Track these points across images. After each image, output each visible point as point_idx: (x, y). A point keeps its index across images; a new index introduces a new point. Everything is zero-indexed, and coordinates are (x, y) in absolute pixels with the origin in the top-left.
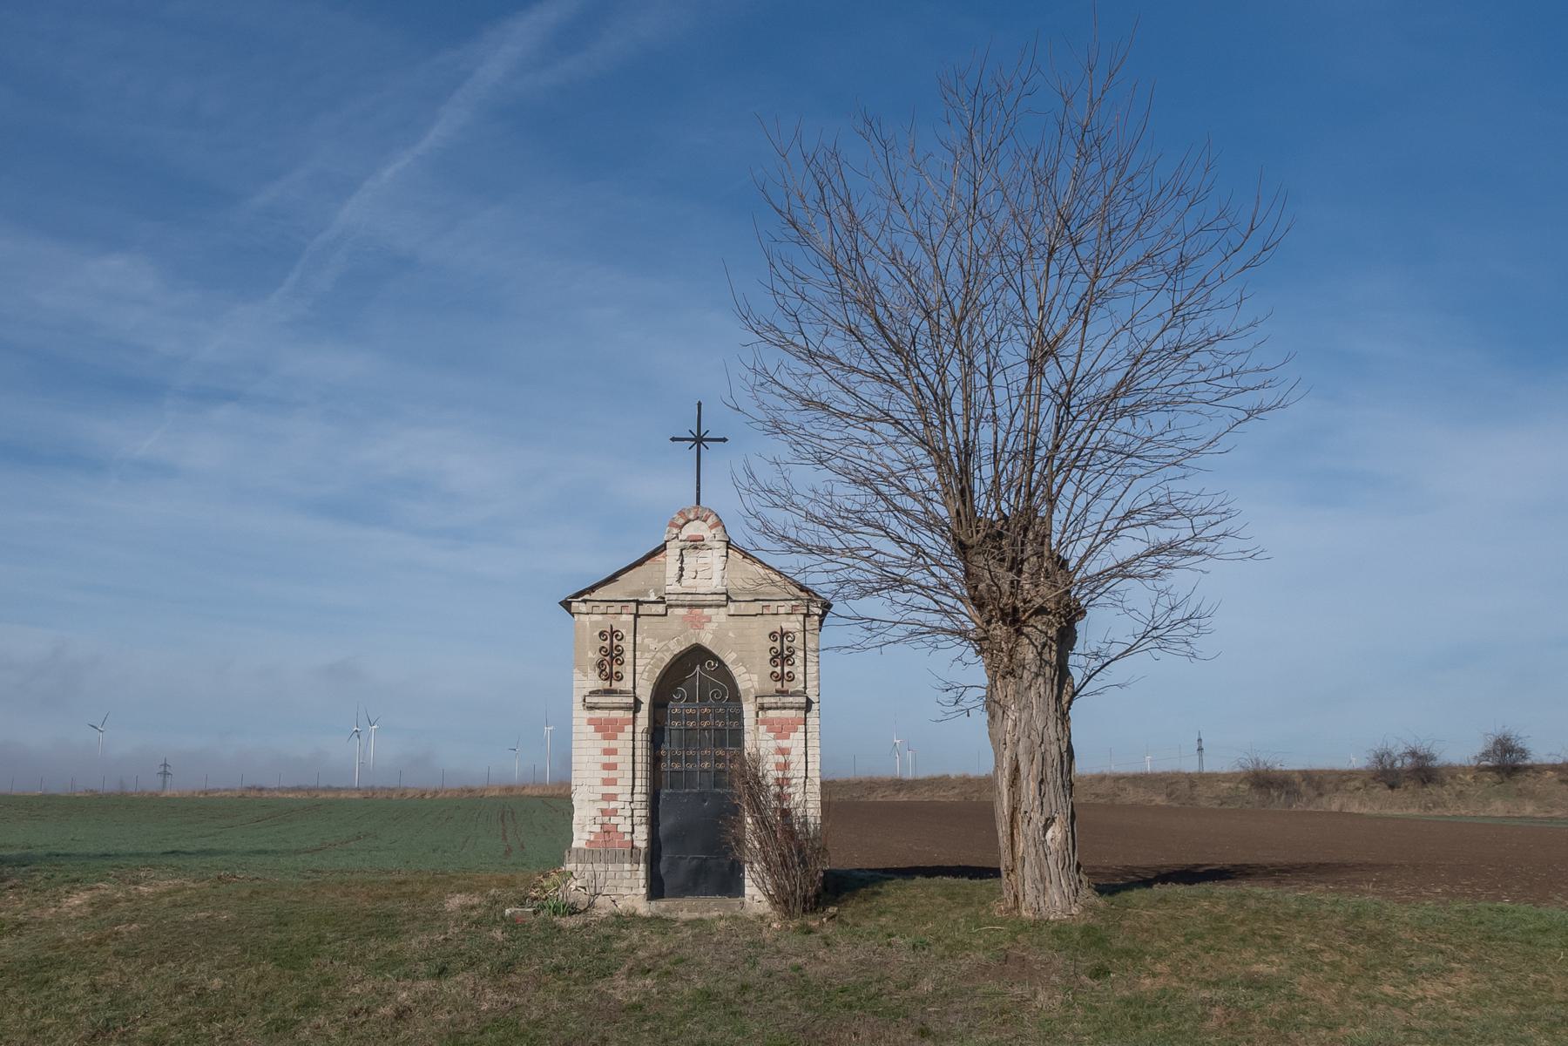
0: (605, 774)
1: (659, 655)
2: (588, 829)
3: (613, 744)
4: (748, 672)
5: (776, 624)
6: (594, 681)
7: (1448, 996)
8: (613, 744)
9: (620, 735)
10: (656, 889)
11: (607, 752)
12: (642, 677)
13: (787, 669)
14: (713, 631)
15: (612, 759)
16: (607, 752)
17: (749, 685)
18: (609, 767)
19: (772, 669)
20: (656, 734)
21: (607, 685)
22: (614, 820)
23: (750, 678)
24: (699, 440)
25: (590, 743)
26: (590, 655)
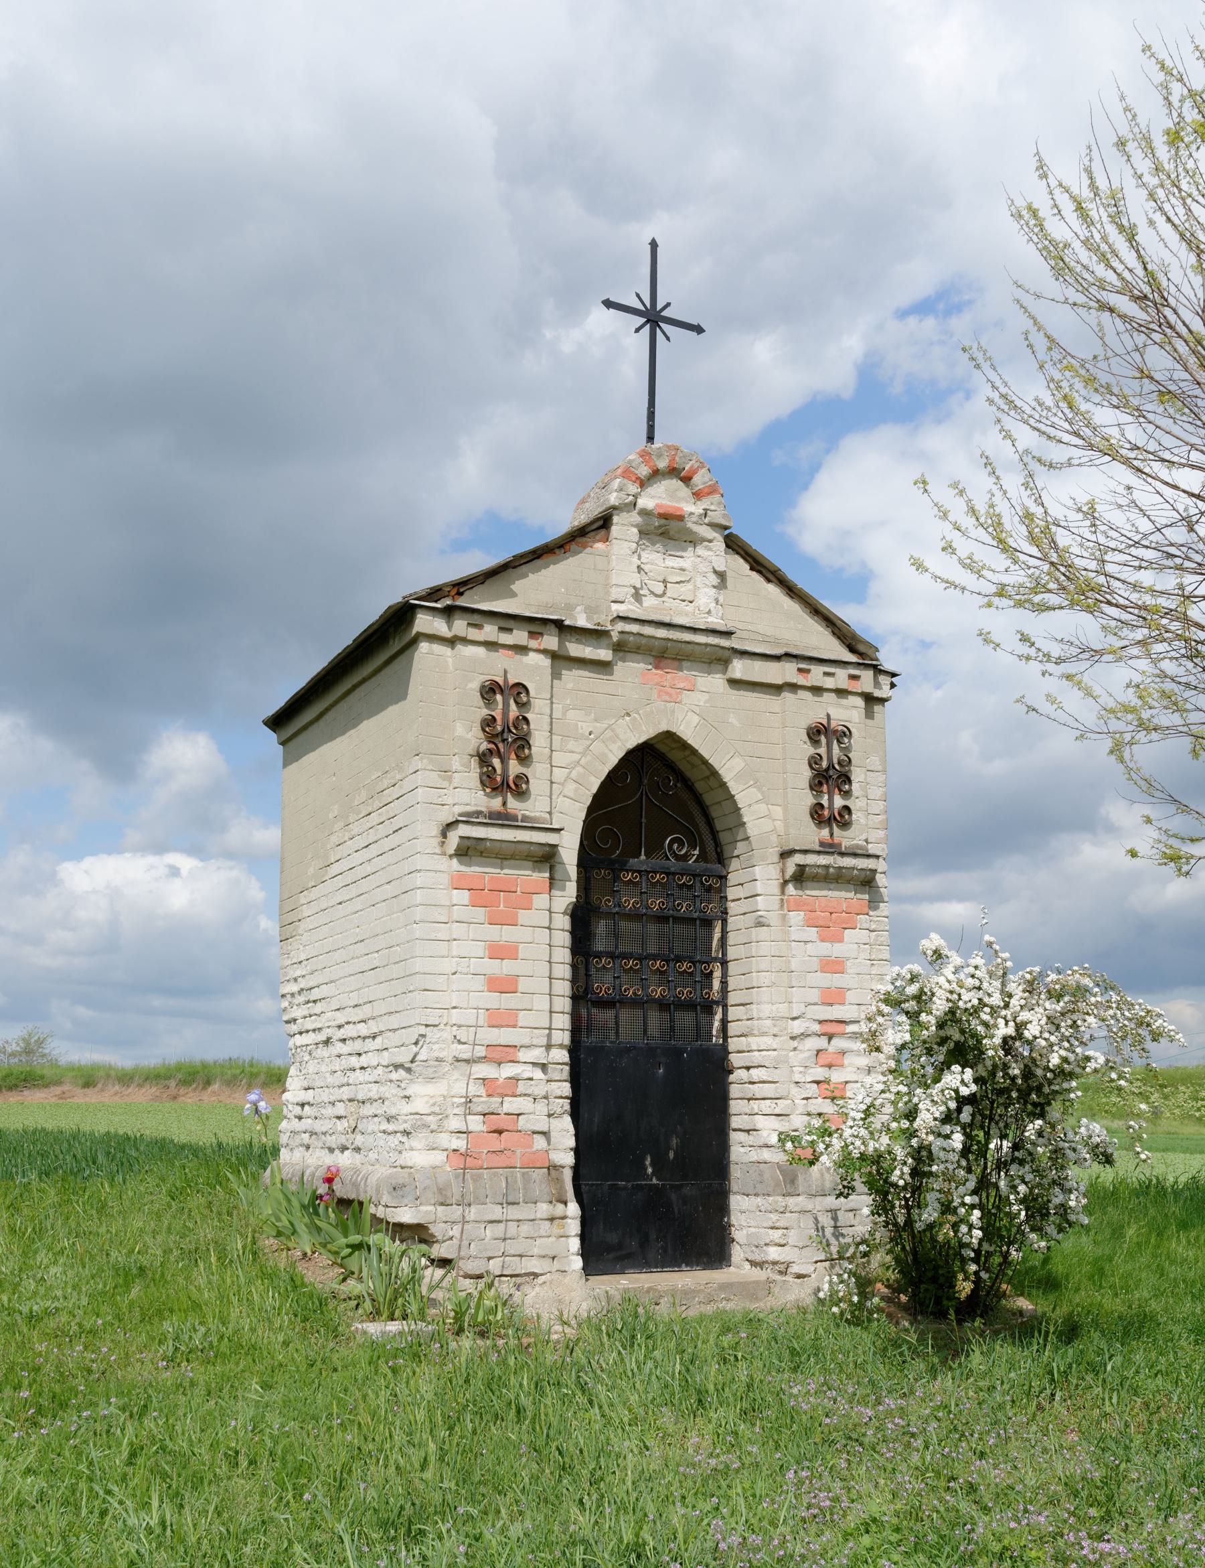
0: (494, 1000)
1: (597, 747)
2: (455, 1123)
3: (837, 950)
4: (765, 800)
5: (816, 710)
6: (467, 793)
7: (681, 1360)
8: (507, 934)
9: (523, 916)
10: (599, 1254)
11: (499, 952)
12: (561, 800)
13: (839, 802)
14: (696, 712)
15: (506, 967)
16: (499, 952)
17: (766, 825)
18: (503, 985)
19: (811, 750)
20: (582, 919)
21: (496, 803)
22: (511, 1105)
23: (768, 805)
24: (653, 318)
25: (457, 930)
26: (460, 730)
